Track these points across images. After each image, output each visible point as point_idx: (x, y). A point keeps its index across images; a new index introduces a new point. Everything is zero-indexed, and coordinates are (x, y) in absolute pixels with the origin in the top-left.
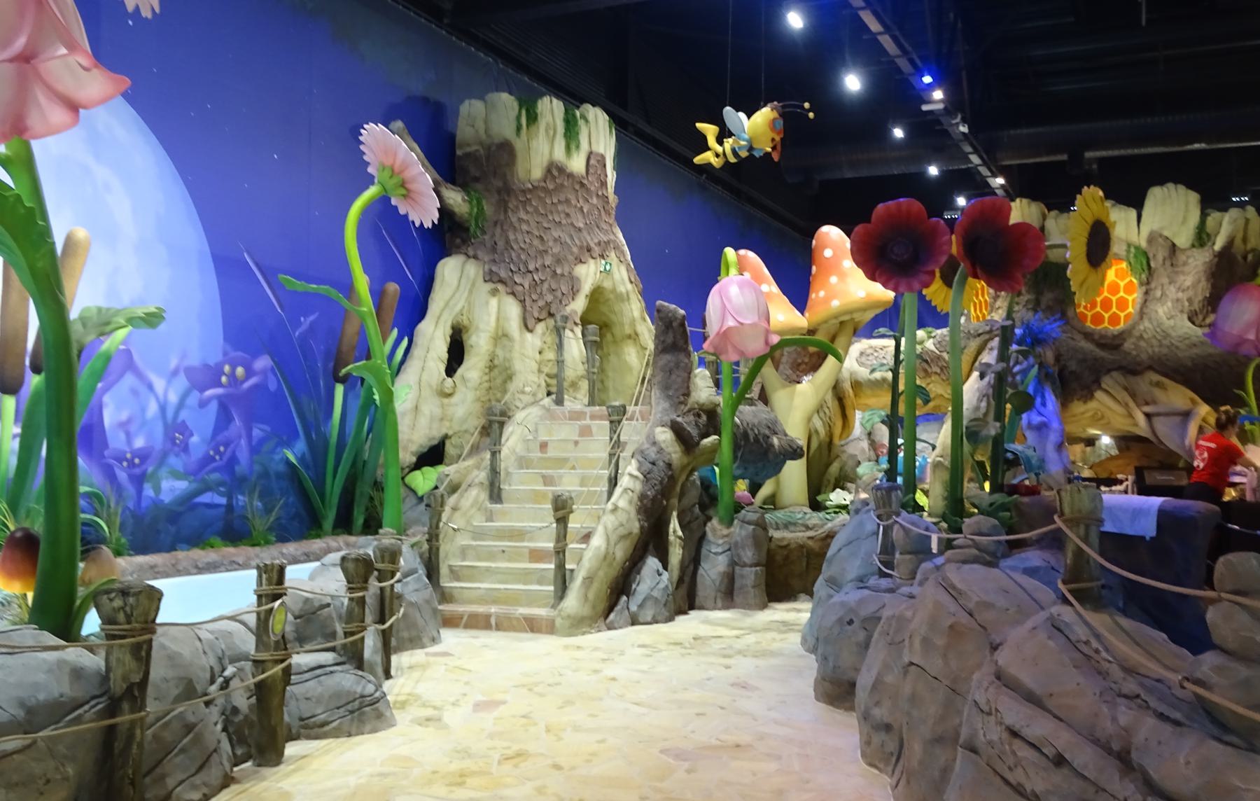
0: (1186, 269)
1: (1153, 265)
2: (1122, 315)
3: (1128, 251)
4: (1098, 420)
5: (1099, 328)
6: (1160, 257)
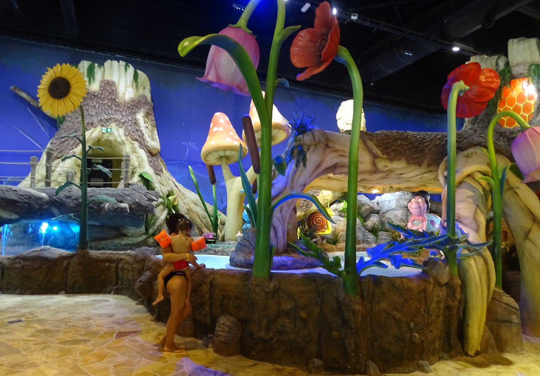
3: (529, 70)
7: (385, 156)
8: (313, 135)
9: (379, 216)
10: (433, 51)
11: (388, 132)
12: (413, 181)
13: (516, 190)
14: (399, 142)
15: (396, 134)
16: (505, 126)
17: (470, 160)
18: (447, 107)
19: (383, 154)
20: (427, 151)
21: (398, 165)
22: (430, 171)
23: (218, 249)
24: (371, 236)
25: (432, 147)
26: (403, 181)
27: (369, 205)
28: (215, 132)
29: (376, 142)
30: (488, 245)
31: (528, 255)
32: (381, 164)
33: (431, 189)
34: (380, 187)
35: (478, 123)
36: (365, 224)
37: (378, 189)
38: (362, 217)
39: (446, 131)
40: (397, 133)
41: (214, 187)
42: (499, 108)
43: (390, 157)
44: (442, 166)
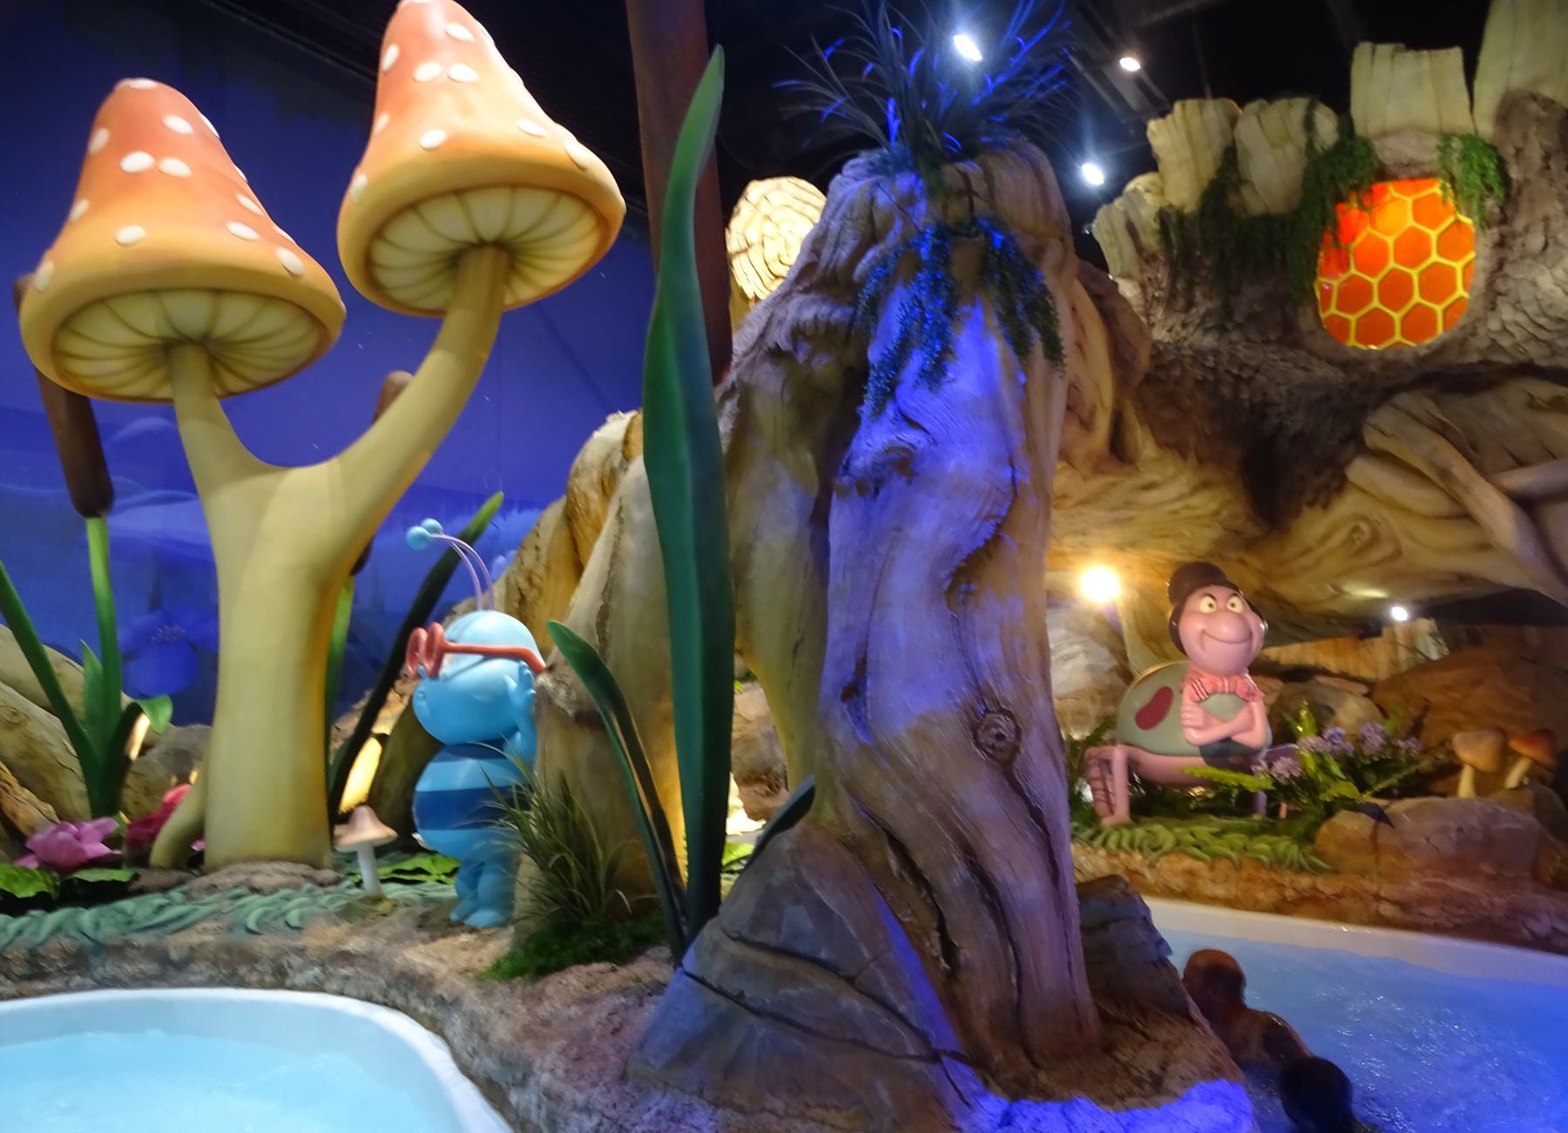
1: (1514, 173)
2: (1439, 309)
3: (1444, 149)
4: (1366, 551)
6: (1535, 153)
16: (1352, 342)
23: (193, 938)
28: (137, 178)
35: (1238, 326)
41: (94, 532)
42: (1322, 279)
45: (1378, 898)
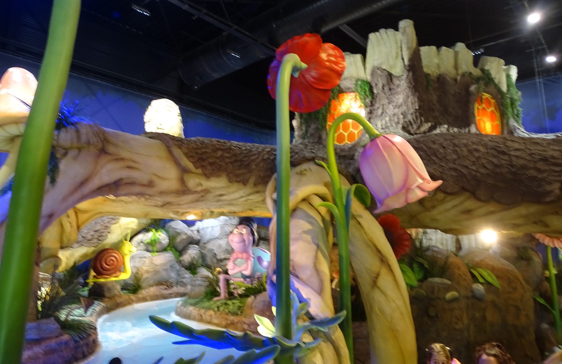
0: (399, 90)
3: (356, 85)
5: (341, 144)
6: (380, 86)
7: (199, 171)
8: (78, 131)
9: (200, 247)
10: (262, 57)
11: (206, 140)
12: (237, 205)
13: (359, 219)
14: (220, 153)
15: (216, 142)
17: (304, 178)
18: (275, 95)
19: (196, 168)
20: (254, 167)
21: (217, 183)
22: (257, 192)
24: (187, 275)
25: (259, 162)
26: (224, 205)
27: (186, 234)
29: (186, 151)
30: (339, 321)
31: (378, 311)
32: (193, 182)
33: (259, 213)
34: (198, 211)
35: (308, 137)
36: (181, 258)
37: (195, 214)
38: (176, 250)
39: (275, 144)
40: (218, 141)
43: (207, 172)
44: (271, 185)
45: (245, 323)
